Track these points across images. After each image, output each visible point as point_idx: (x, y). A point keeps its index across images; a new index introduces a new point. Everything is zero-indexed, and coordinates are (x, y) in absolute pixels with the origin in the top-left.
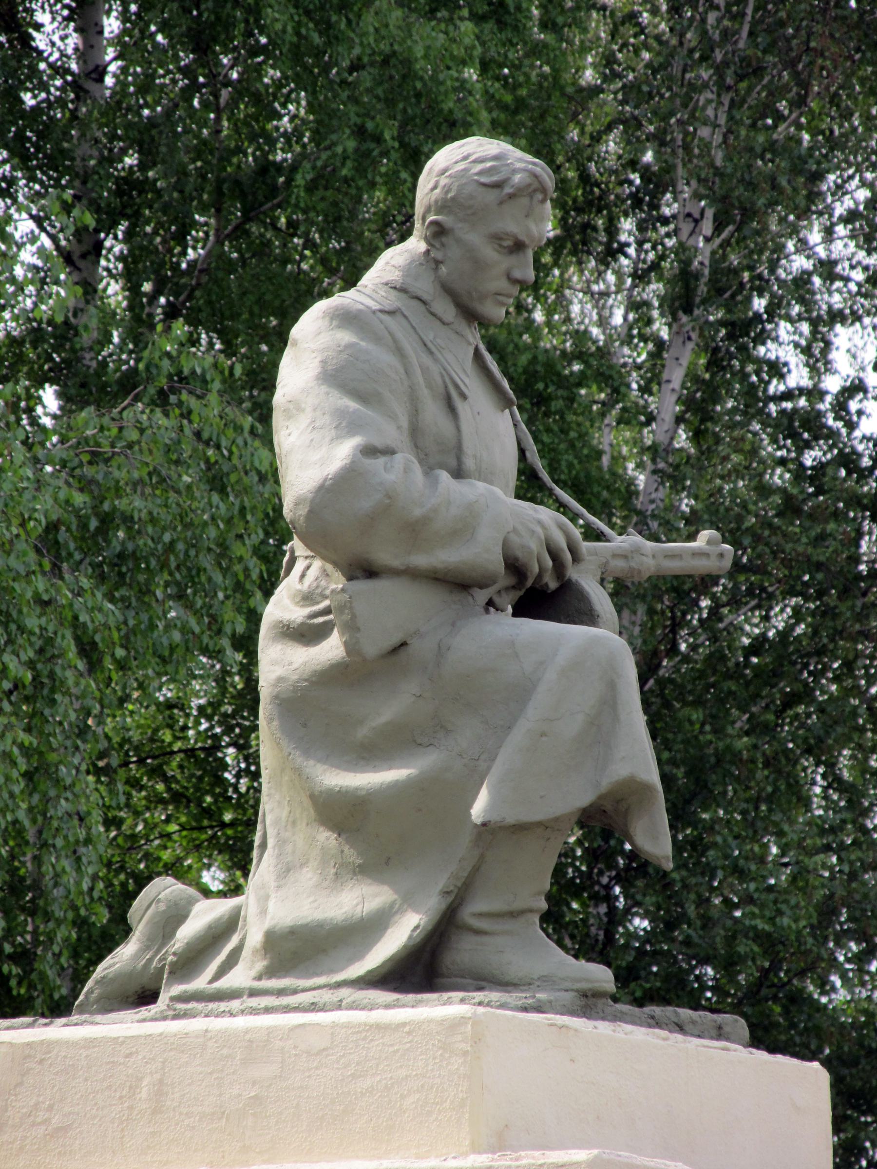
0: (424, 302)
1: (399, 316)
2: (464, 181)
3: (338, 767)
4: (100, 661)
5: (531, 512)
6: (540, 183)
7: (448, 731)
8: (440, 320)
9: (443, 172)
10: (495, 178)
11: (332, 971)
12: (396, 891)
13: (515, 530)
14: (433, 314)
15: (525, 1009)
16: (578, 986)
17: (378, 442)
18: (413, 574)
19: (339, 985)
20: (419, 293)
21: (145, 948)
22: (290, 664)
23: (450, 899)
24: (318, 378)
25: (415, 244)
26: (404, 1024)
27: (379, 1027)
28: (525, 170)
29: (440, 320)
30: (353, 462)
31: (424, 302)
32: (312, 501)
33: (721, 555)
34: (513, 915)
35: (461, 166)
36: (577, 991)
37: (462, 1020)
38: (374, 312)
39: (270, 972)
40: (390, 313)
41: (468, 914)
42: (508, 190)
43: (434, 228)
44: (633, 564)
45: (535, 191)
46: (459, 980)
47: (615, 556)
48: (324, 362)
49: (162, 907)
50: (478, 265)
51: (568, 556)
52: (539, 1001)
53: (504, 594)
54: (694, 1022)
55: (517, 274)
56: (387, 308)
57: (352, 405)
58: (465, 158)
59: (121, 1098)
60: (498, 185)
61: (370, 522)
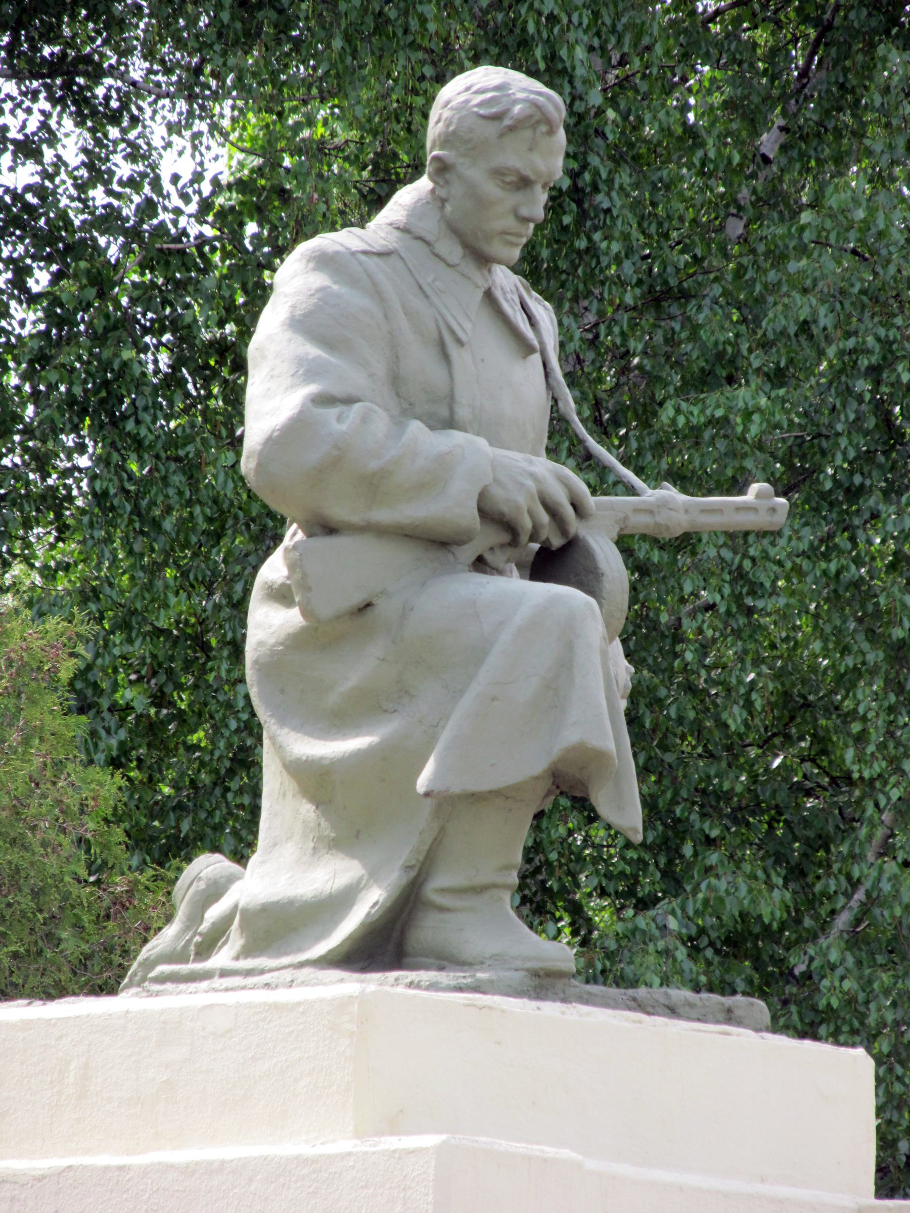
0: (427, 243)
1: (394, 257)
2: (464, 113)
3: (311, 735)
5: (524, 464)
6: (543, 114)
7: (412, 696)
9: (448, 103)
10: (494, 110)
11: (300, 950)
12: (365, 866)
13: (496, 480)
14: (437, 256)
15: (460, 989)
16: (528, 965)
17: (338, 390)
18: (380, 531)
20: (423, 234)
21: (186, 929)
22: (270, 627)
23: (413, 874)
24: (283, 324)
25: (424, 183)
26: (299, 1004)
27: (277, 1007)
30: (301, 412)
31: (427, 243)
32: (261, 452)
33: (773, 510)
34: (479, 890)
35: (462, 98)
36: (528, 970)
38: (353, 254)
39: (246, 952)
40: (383, 254)
41: (431, 890)
42: (507, 122)
43: (437, 165)
44: (659, 519)
45: (538, 122)
46: (423, 960)
47: (637, 510)
48: (293, 307)
49: (202, 885)
50: (481, 203)
51: (570, 511)
52: (478, 980)
53: (498, 552)
54: (691, 1005)
55: (524, 212)
56: (377, 248)
57: (313, 351)
58: (468, 89)
59: (51, 1082)
60: (497, 117)
61: (321, 473)
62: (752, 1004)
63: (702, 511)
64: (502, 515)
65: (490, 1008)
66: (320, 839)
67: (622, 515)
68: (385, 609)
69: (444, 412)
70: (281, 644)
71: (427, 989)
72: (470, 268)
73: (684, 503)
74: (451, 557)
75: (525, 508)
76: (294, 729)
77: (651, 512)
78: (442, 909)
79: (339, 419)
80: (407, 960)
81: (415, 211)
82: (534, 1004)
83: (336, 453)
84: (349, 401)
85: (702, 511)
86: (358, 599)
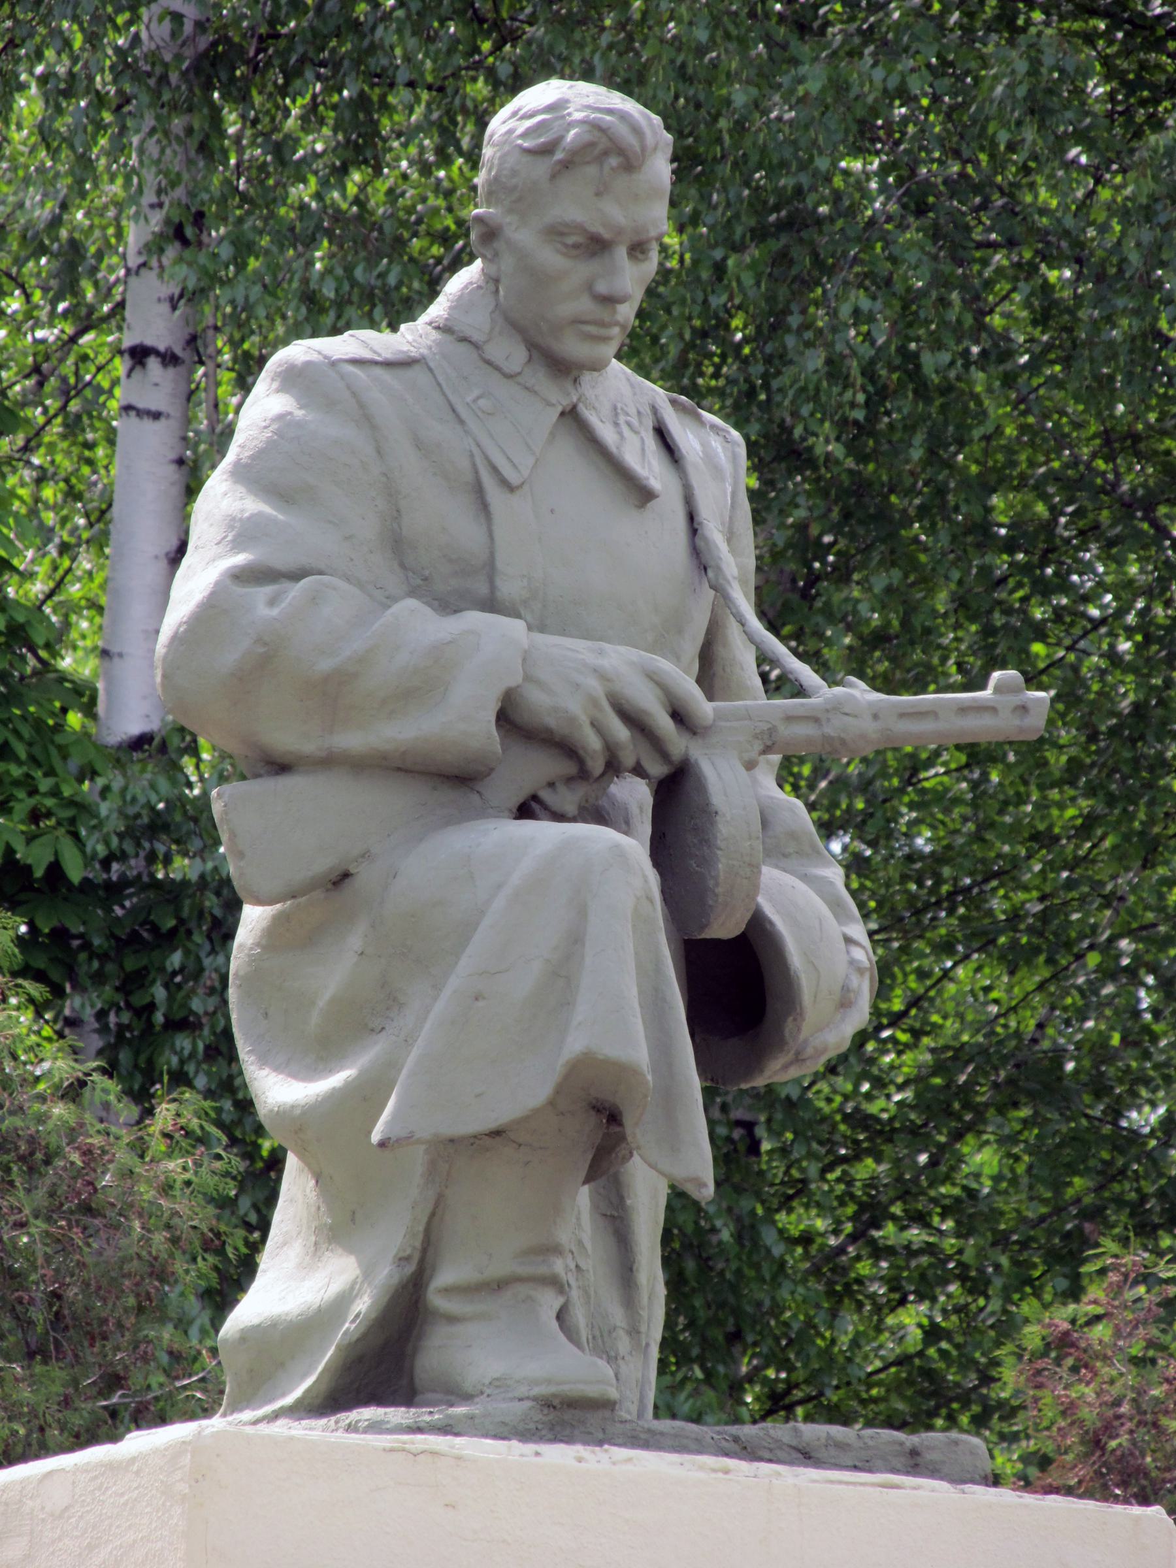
0: (476, 346)
2: (507, 148)
4: (891, 988)
5: (591, 659)
7: (401, 1005)
8: (498, 369)
14: (488, 363)
17: (282, 560)
18: (328, 762)
19: (276, 1416)
20: (468, 332)
23: (410, 1268)
26: (133, 1460)
28: (583, 122)
29: (498, 369)
31: (476, 346)
33: (1023, 709)
36: (535, 1399)
37: (183, 1445)
38: (334, 364)
42: (559, 155)
44: (829, 730)
45: (606, 153)
47: (790, 719)
50: (539, 280)
51: (664, 723)
52: (449, 1417)
54: (842, 1446)
60: (546, 150)
62: (956, 1443)
63: (902, 715)
64: (549, 731)
65: (434, 1453)
66: (318, 1230)
67: (765, 726)
68: (366, 877)
69: (483, 589)
70: (258, 945)
71: (366, 1431)
72: (539, 378)
73: (870, 704)
74: (475, 798)
75: (584, 720)
76: (277, 1069)
77: (817, 720)
78: (452, 1319)
79: (272, 602)
80: (418, 1398)
81: (461, 303)
82: (530, 1448)
83: (262, 650)
84: (296, 575)
85: (902, 715)
86: (323, 864)
